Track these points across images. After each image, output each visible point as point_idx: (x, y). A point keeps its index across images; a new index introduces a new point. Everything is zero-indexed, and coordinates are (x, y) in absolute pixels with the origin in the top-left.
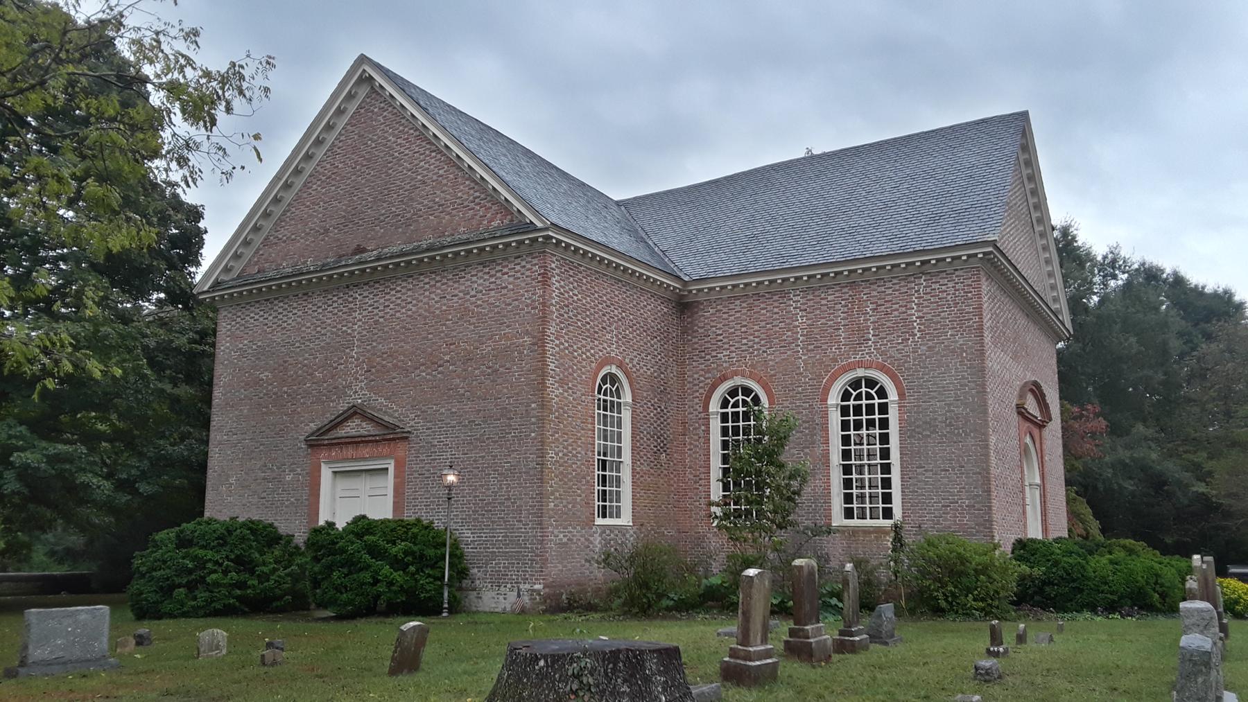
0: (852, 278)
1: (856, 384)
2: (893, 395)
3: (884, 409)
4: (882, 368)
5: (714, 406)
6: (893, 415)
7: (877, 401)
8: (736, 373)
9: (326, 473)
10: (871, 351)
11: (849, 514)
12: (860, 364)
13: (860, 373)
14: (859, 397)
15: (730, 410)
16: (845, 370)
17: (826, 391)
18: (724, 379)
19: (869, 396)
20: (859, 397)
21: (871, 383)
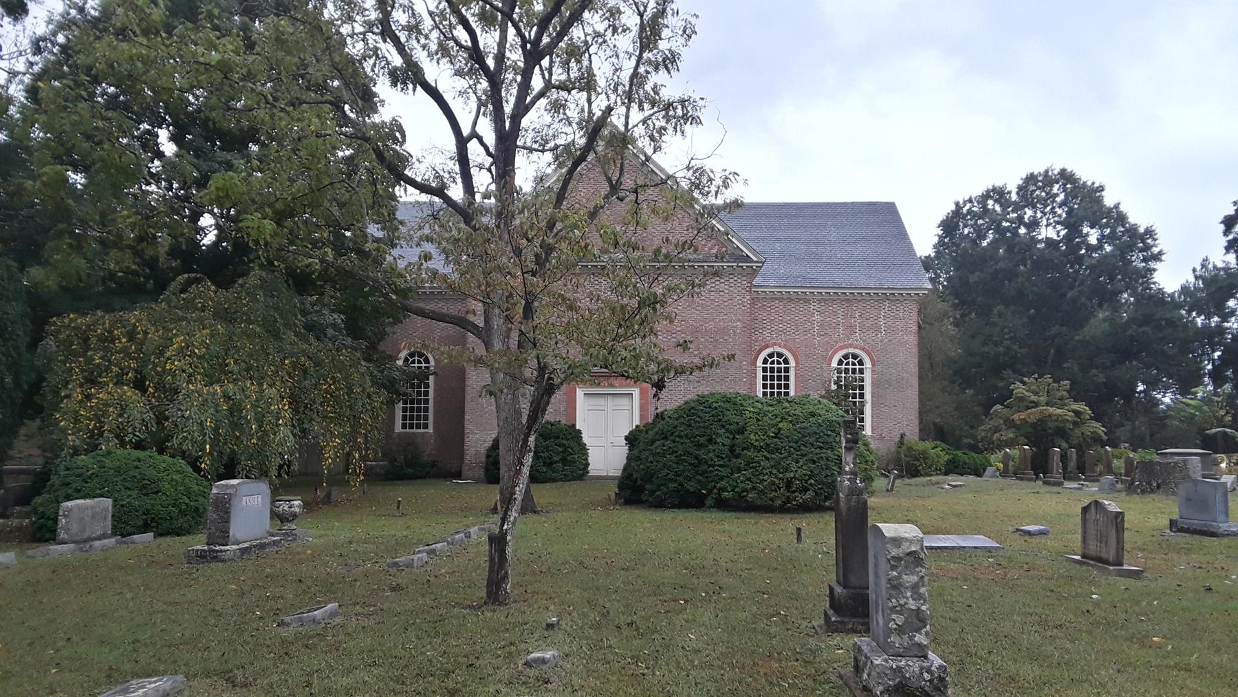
0: (849, 298)
1: (846, 357)
2: (792, 364)
3: (787, 370)
4: (863, 349)
5: (760, 363)
6: (792, 374)
7: (858, 367)
8: (775, 344)
9: (580, 393)
10: (857, 339)
11: (404, 426)
12: (851, 346)
13: (851, 350)
14: (848, 364)
15: (768, 365)
16: (842, 348)
17: (831, 358)
18: (767, 347)
19: (854, 364)
20: (848, 364)
21: (780, 355)
